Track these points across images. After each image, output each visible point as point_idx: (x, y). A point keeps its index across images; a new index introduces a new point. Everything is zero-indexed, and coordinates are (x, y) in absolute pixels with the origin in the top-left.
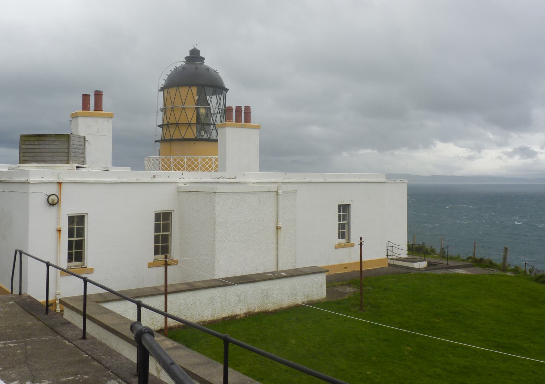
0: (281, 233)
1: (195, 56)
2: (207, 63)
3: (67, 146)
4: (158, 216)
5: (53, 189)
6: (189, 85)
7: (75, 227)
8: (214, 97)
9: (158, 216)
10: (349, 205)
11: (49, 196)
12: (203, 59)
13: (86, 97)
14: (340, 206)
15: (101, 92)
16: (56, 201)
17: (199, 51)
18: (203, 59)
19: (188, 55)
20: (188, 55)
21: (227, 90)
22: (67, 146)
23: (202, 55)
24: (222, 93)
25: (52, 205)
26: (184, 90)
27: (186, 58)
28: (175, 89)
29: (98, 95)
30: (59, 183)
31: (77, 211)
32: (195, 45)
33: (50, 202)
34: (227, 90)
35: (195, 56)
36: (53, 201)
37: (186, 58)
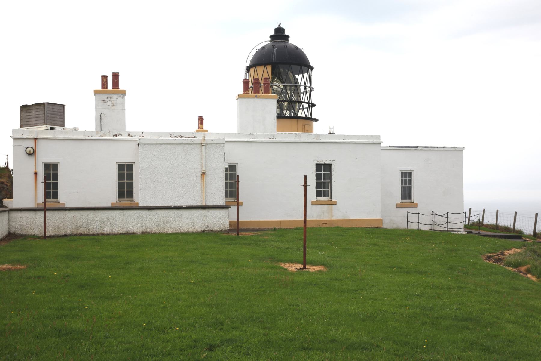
0: (207, 178)
1: (279, 35)
2: (291, 41)
3: (43, 112)
4: (121, 167)
5: (31, 144)
6: (265, 64)
7: (52, 172)
8: (301, 76)
9: (121, 167)
10: (330, 165)
11: (27, 148)
12: (288, 37)
13: (104, 78)
14: (317, 165)
15: (118, 73)
16: (32, 151)
17: (284, 29)
18: (288, 37)
19: (273, 33)
20: (273, 33)
21: (312, 68)
22: (43, 112)
23: (286, 33)
24: (308, 72)
25: (30, 154)
26: (260, 69)
27: (271, 37)
28: (254, 68)
29: (116, 76)
30: (35, 139)
31: (51, 160)
32: (279, 23)
33: (28, 152)
34: (312, 68)
35: (279, 35)
36: (30, 151)
37: (271, 37)
